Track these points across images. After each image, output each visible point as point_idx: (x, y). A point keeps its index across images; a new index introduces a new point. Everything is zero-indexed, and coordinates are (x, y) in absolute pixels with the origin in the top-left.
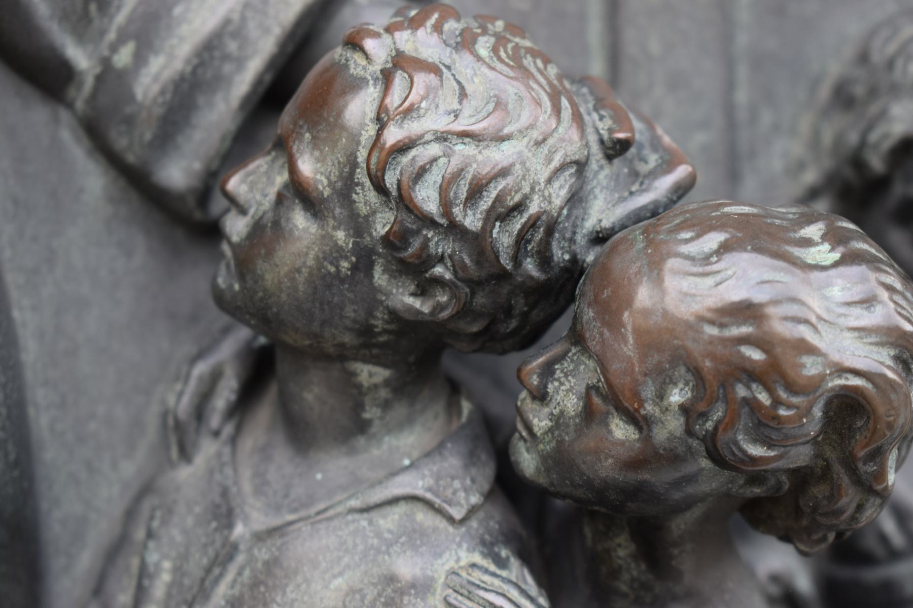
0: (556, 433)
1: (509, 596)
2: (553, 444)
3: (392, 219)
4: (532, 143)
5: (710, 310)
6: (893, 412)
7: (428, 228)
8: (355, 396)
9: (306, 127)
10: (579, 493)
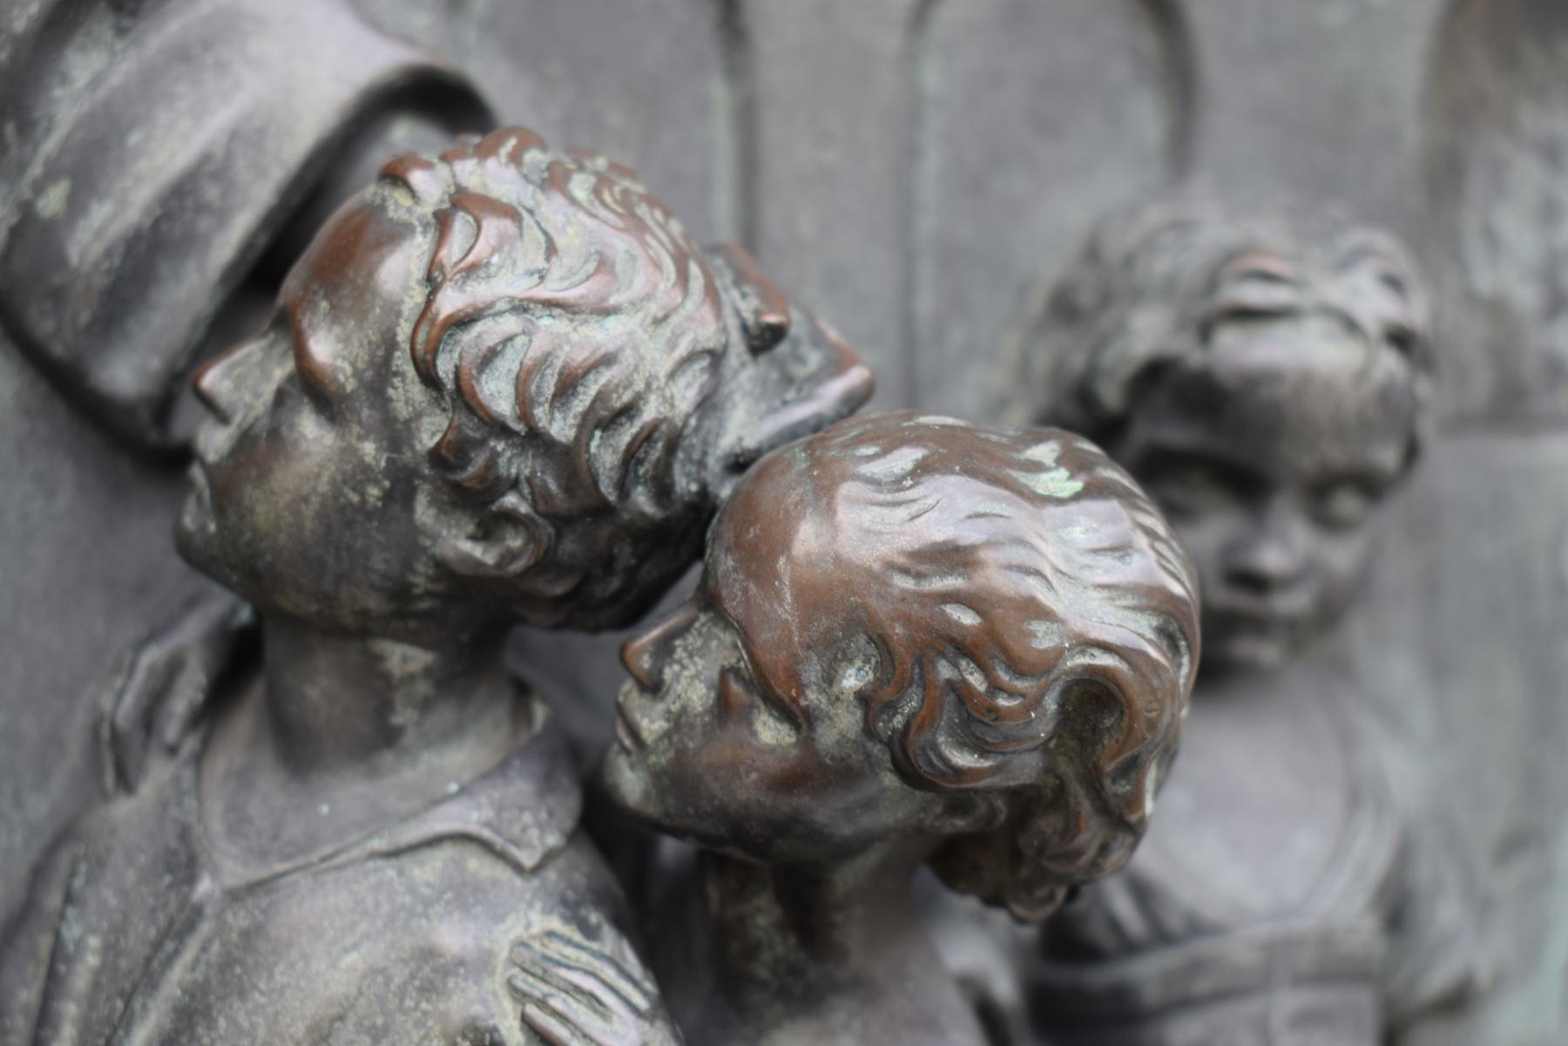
0: (675, 738)
1: (603, 976)
2: (671, 754)
3: (445, 425)
4: (649, 320)
5: (902, 553)
6: (1155, 705)
7: (498, 437)
8: (379, 691)
9: (321, 293)
10: (707, 827)
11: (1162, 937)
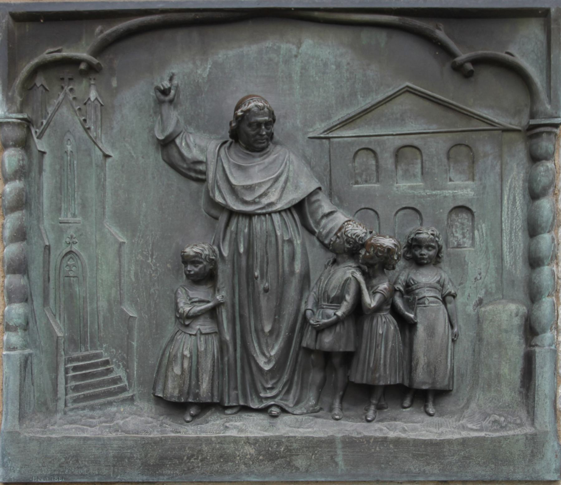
11: (415, 284)
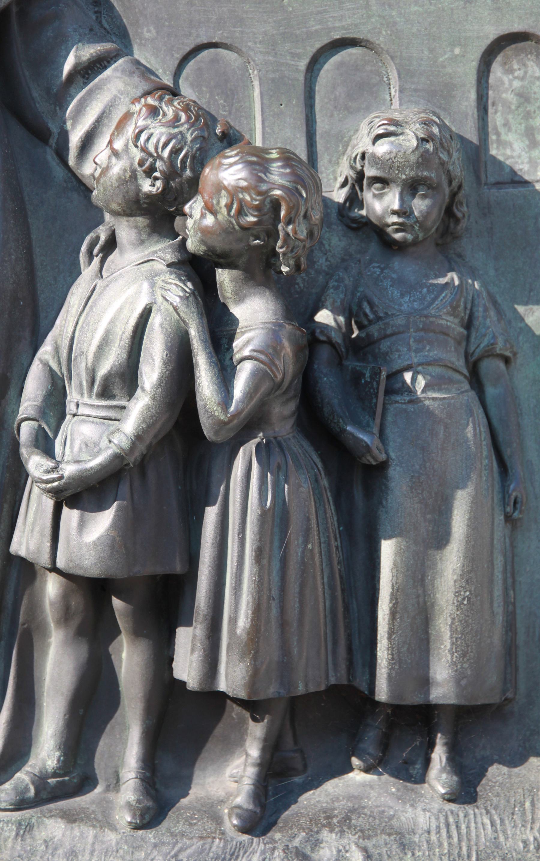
11: (379, 319)
